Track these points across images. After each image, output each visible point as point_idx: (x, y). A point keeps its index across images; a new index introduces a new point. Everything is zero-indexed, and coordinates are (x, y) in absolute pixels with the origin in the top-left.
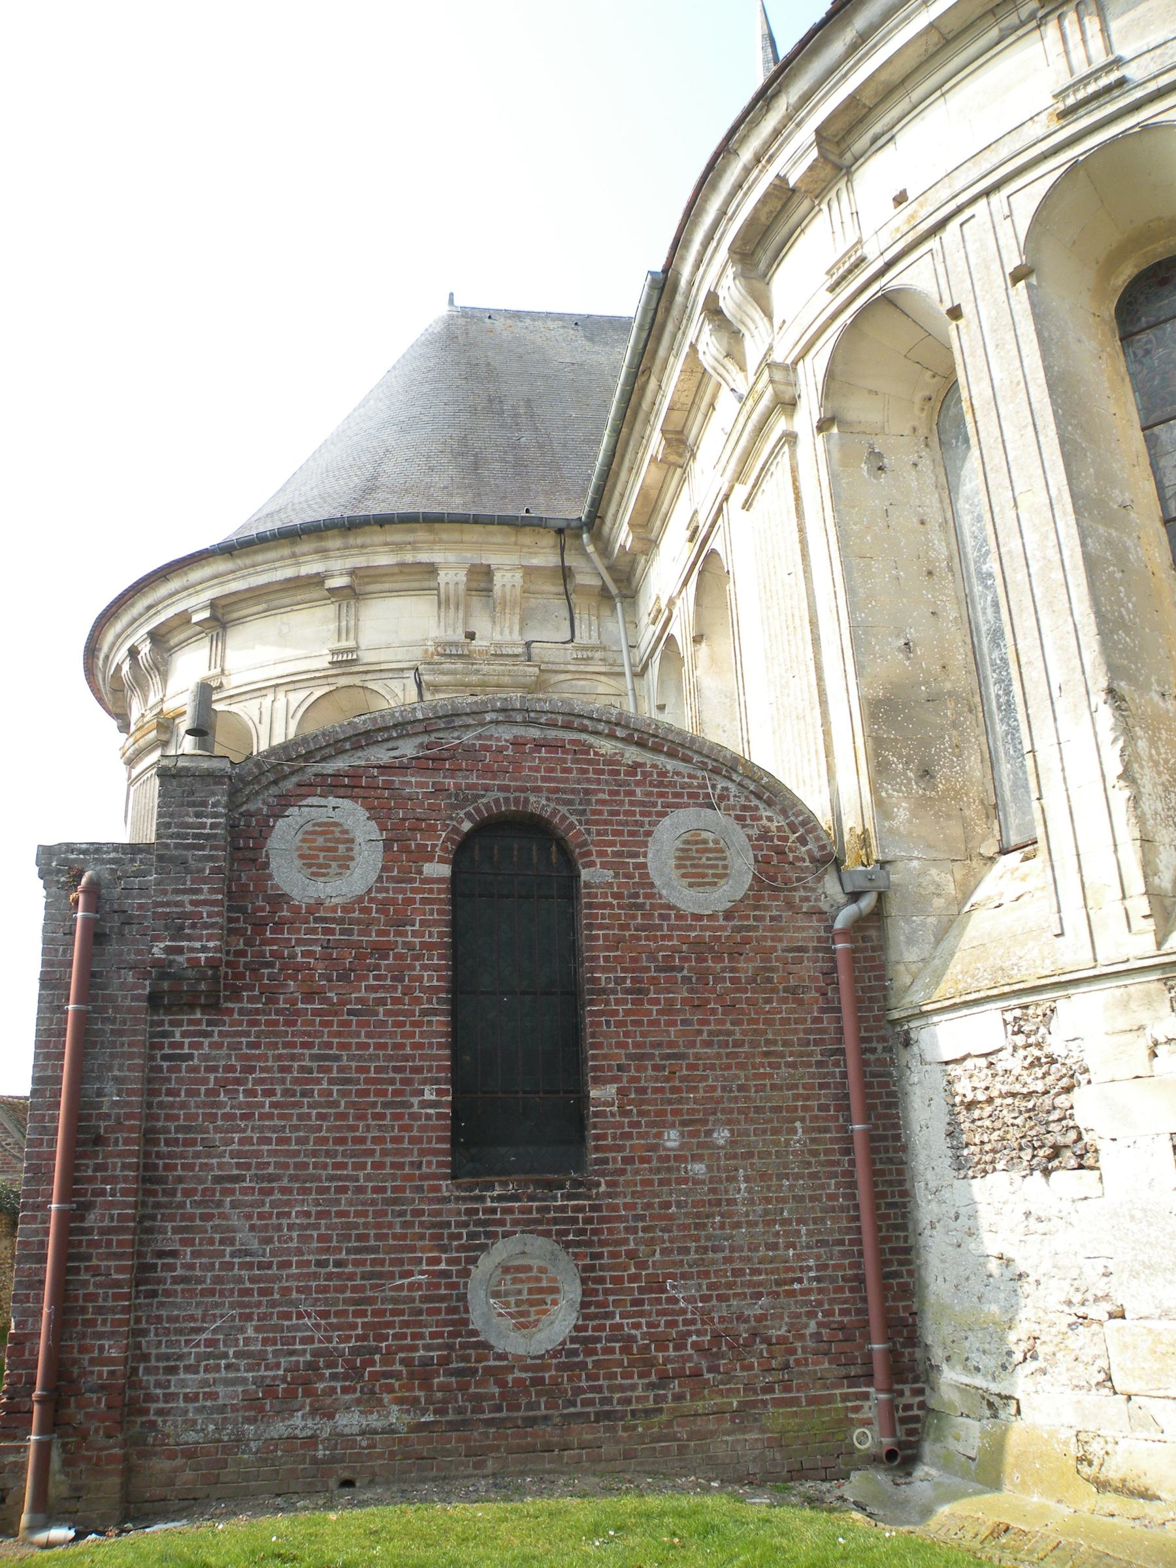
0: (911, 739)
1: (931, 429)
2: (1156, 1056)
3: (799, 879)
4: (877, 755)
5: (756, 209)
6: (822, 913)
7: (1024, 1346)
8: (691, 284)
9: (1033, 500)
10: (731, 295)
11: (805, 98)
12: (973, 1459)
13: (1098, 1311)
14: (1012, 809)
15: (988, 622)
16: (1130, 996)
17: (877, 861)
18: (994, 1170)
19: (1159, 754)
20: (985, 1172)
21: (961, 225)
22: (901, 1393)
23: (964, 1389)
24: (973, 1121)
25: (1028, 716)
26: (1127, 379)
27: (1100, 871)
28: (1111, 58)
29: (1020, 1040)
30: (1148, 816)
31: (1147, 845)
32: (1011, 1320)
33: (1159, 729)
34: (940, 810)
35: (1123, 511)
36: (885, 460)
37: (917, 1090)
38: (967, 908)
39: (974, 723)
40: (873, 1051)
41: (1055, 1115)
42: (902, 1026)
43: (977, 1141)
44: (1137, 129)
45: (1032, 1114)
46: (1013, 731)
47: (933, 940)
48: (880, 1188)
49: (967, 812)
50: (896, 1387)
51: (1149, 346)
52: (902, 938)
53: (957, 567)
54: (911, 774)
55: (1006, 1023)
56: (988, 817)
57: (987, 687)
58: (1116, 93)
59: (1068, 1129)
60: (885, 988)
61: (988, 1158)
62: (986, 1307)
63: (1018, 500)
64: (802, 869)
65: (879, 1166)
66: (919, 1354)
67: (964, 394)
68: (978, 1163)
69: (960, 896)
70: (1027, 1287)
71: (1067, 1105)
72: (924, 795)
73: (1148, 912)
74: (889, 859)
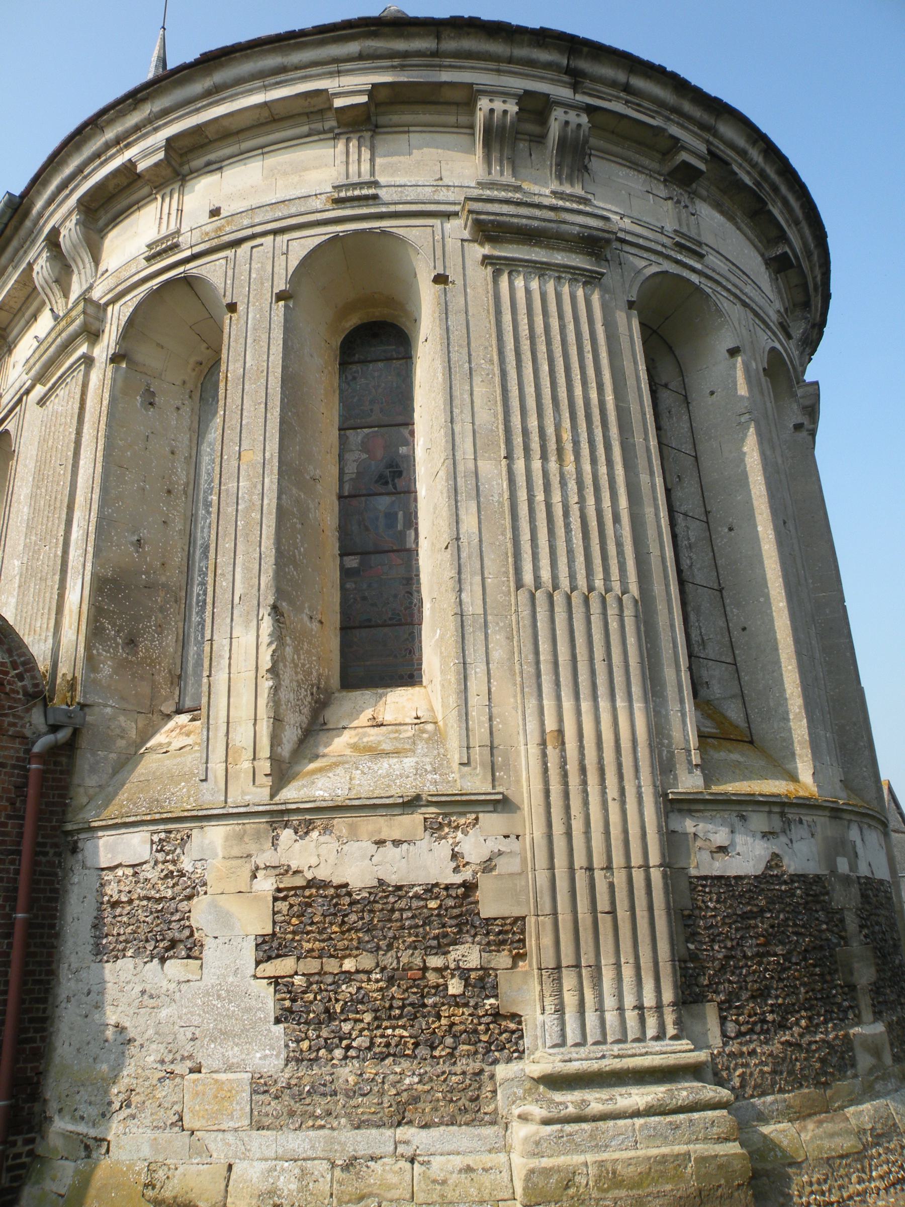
0: (126, 614)
1: (196, 387)
2: (256, 877)
3: (10, 708)
4: (96, 621)
5: (107, 178)
6: (24, 737)
7: (122, 1097)
8: (40, 215)
9: (252, 457)
10: (69, 234)
11: (165, 112)
12: (62, 1196)
13: (181, 1068)
14: (191, 681)
15: (203, 538)
16: (245, 832)
17: (79, 703)
18: (124, 956)
19: (299, 659)
20: (117, 957)
21: (252, 248)
22: (14, 1144)
23: (68, 1136)
24: (115, 917)
25: (213, 613)
26: (338, 392)
27: (242, 736)
28: (372, 179)
29: (160, 856)
30: (283, 703)
31: (277, 723)
32: (116, 1076)
33: (303, 641)
34: (136, 672)
35: (312, 482)
36: (157, 399)
37: (76, 889)
38: (142, 751)
39: (177, 611)
40: (45, 854)
41: (177, 917)
42: (73, 836)
43: (115, 933)
44: (378, 231)
45: (159, 914)
46: (202, 623)
47: (110, 771)
48: (31, 967)
49: (157, 677)
50: (12, 1138)
51: (356, 375)
52: (87, 767)
53: (190, 491)
54: (120, 641)
55: (152, 843)
56: (172, 684)
57: (192, 587)
58: (371, 202)
59: (184, 927)
60: (66, 805)
61: (120, 947)
62: (98, 1067)
63: (242, 454)
64: (15, 700)
65: (32, 949)
66: (37, 1107)
67: (223, 368)
68: (113, 950)
69: (138, 740)
70: (133, 1050)
71: (187, 909)
72: (127, 658)
73: (269, 772)
74: (89, 702)
